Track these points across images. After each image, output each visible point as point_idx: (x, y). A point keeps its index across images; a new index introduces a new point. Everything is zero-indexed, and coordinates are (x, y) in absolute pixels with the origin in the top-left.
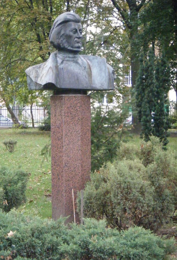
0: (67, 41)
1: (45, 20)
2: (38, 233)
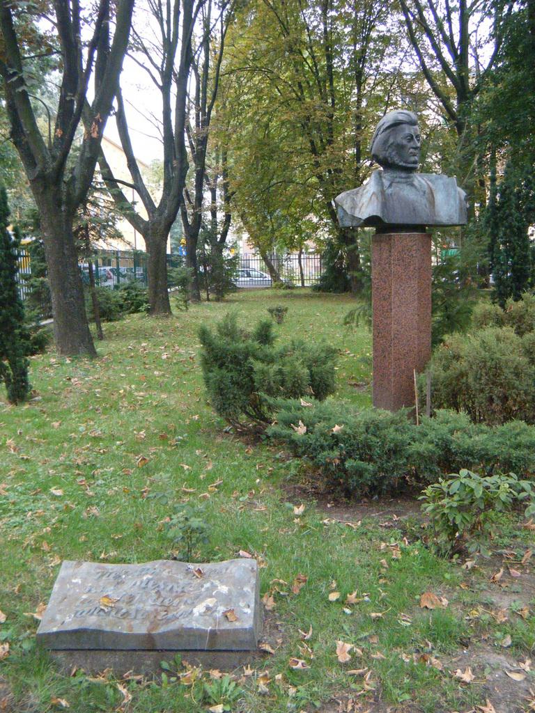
1: (325, 119)
2: (374, 428)
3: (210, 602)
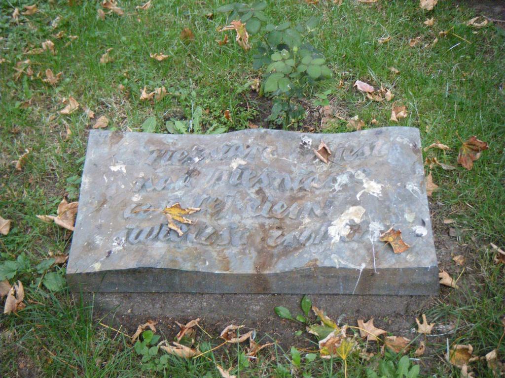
3: (354, 214)
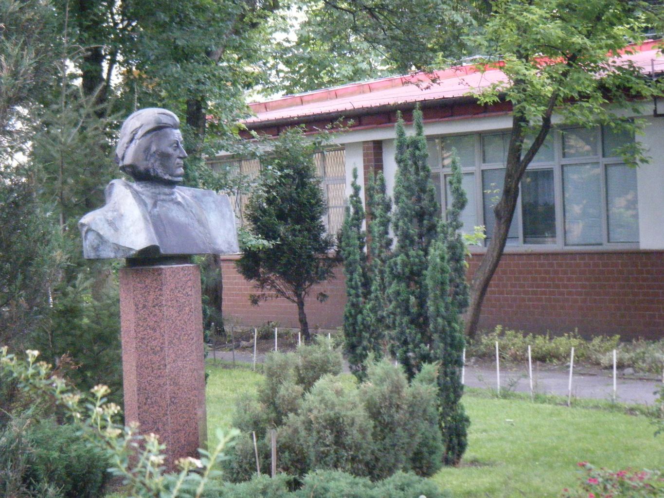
0: (161, 164)
